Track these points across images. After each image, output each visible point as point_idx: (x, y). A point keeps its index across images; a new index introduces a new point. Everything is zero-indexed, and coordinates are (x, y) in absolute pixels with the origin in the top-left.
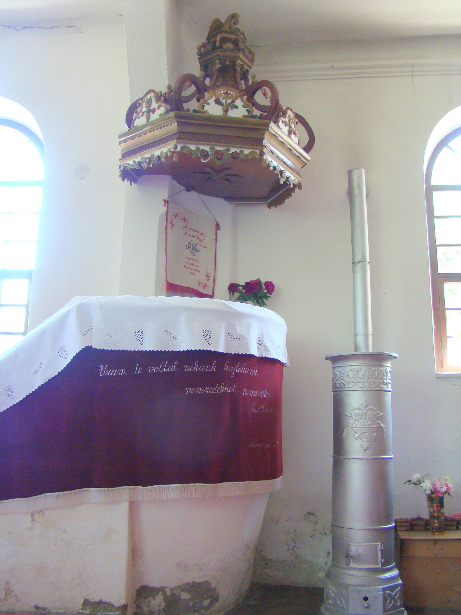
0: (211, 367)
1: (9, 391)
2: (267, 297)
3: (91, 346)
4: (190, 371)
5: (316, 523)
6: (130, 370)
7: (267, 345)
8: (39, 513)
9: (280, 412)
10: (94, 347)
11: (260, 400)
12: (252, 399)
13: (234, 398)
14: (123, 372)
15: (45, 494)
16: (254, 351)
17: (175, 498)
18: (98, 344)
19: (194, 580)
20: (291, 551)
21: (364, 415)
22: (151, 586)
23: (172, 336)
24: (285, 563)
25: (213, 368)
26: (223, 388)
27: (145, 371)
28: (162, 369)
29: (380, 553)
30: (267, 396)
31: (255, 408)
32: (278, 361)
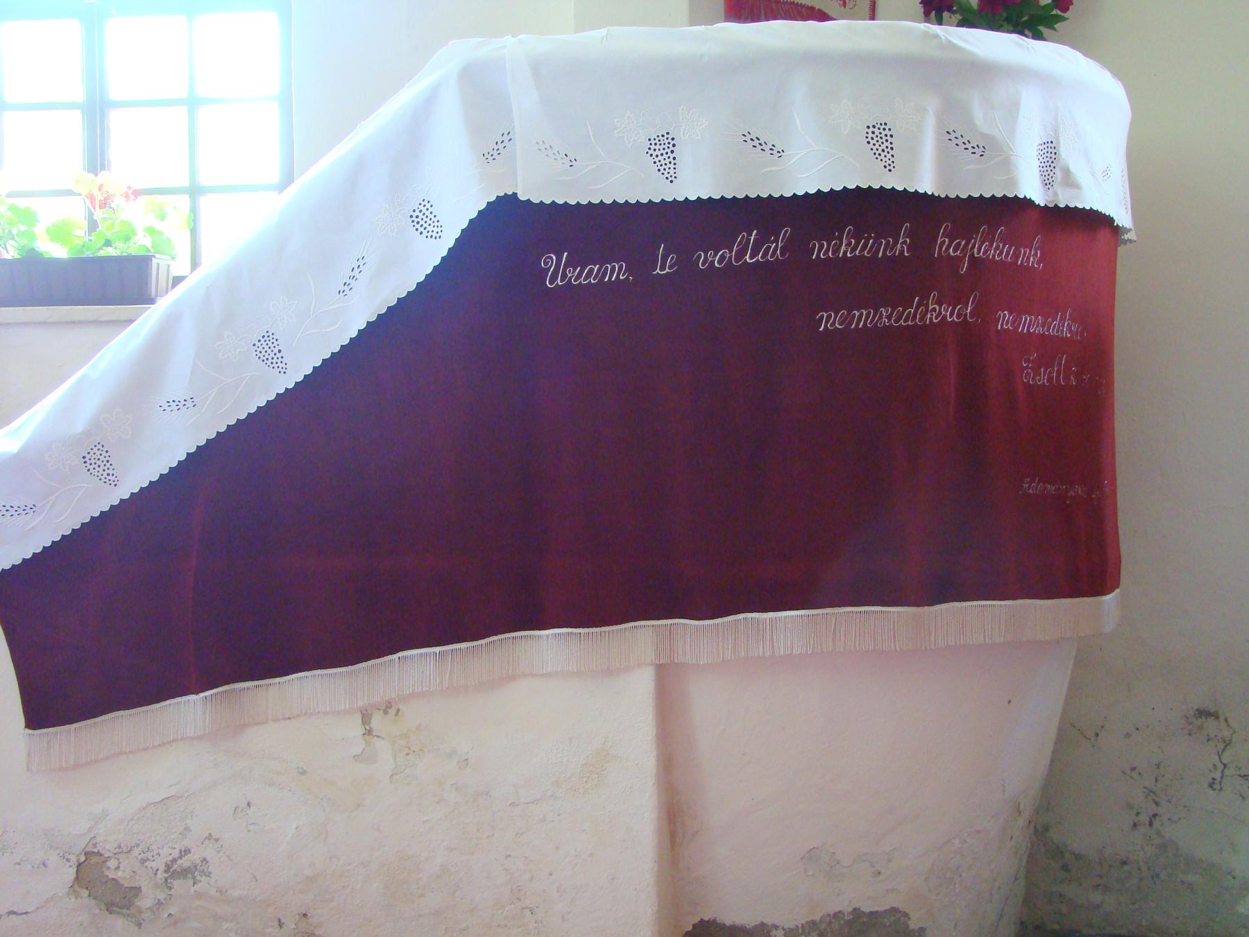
0: (896, 242)
1: (269, 350)
2: (1059, 19)
3: (515, 195)
5: (1227, 743)
6: (640, 264)
7: (1072, 168)
8: (386, 712)
9: (1110, 384)
10: (522, 197)
11: (1048, 348)
12: (1026, 340)
13: (971, 339)
14: (616, 272)
15: (401, 654)
16: (1032, 189)
17: (796, 651)
18: (537, 187)
19: (857, 906)
20: (1142, 829)
22: (728, 923)
23: (767, 148)
24: (1126, 868)
25: (902, 246)
26: (934, 310)
27: (686, 264)
30: (1070, 331)
31: (1037, 373)
32: (1107, 221)
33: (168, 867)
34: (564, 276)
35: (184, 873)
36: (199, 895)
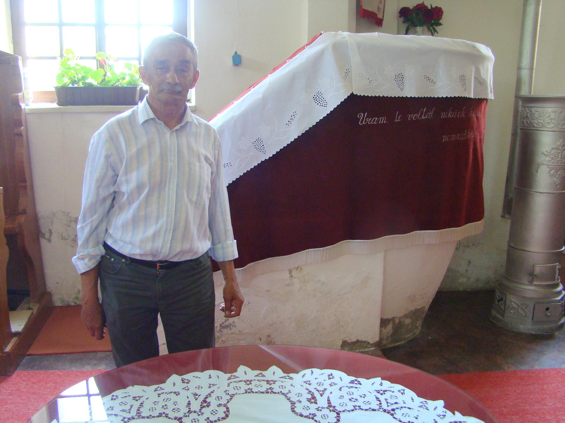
1: (259, 145)
4: (445, 118)
8: (297, 269)
14: (383, 120)
21: (560, 154)
28: (421, 116)
29: (557, 271)
33: (221, 325)
34: (366, 121)
35: (227, 327)
36: (232, 333)
